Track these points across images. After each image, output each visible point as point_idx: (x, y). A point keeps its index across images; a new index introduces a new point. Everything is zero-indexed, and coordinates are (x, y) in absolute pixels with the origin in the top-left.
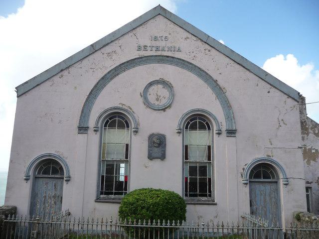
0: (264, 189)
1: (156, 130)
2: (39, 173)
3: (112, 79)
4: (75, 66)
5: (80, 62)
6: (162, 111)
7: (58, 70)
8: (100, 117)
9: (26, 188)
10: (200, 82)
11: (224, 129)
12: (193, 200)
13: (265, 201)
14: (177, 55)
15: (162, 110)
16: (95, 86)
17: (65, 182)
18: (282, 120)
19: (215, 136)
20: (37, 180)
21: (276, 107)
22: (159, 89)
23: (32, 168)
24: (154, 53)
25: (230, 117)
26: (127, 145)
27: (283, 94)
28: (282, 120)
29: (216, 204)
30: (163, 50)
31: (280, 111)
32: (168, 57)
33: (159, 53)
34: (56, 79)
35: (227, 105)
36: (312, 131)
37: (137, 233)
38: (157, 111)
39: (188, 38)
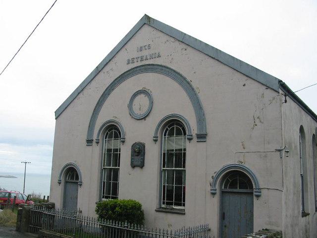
0: (235, 201)
2: (225, 187)
3: (109, 94)
4: (87, 87)
7: (76, 94)
9: (60, 190)
17: (255, 198)
22: (142, 100)
23: (218, 182)
24: (140, 64)
27: (260, 85)
28: (258, 118)
30: (147, 59)
37: (109, 230)
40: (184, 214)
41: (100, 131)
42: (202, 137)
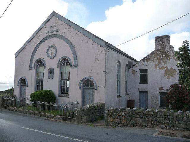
1: (51, 67)
10: (66, 44)
12: (63, 95)
13: (90, 97)
14: (59, 33)
18: (97, 58)
20: (85, 89)
25: (76, 59)
29: (69, 97)
32: (55, 35)
33: (53, 34)
34: (24, 50)
35: (75, 53)
36: (172, 58)
39: (62, 24)
40: (69, 97)
41: (35, 63)
42: (76, 66)
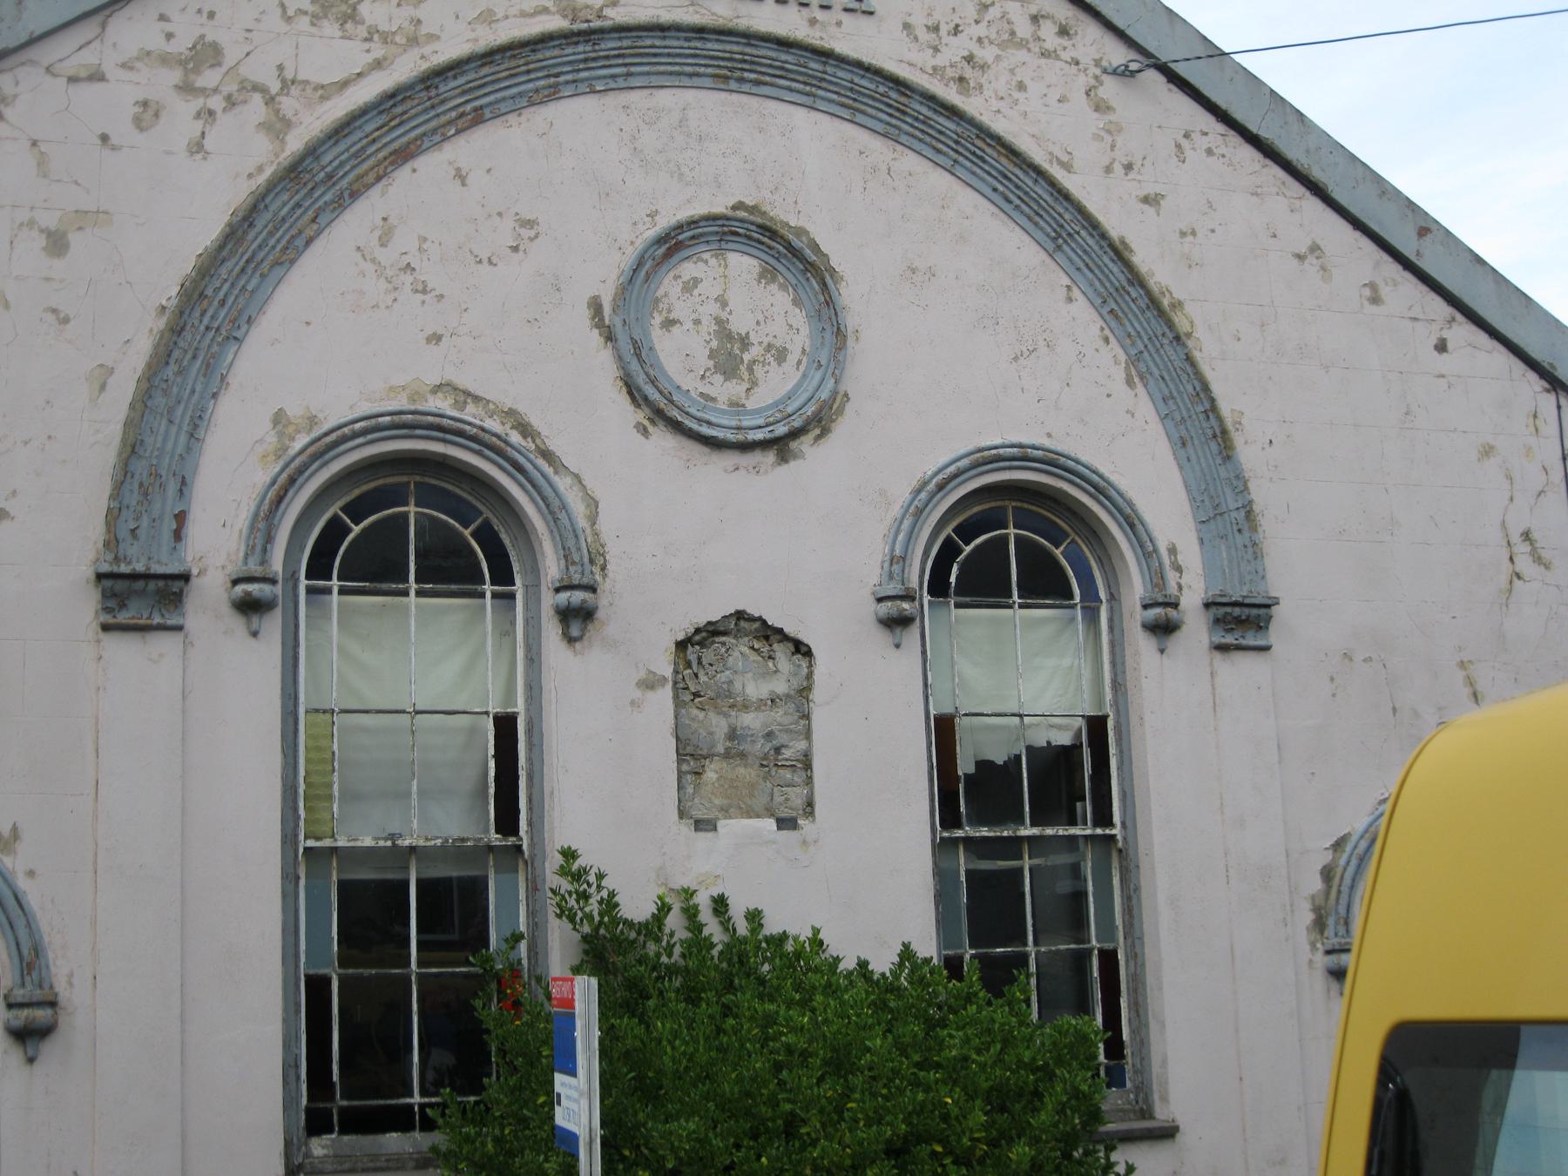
5: (88, 30)
6: (770, 457)
8: (279, 500)
11: (1193, 592)
15: (764, 445)
16: (234, 234)
18: (1527, 536)
19: (1142, 645)
21: (1487, 451)
26: (505, 726)
27: (1518, 366)
31: (1510, 478)
32: (784, 44)
38: (731, 459)
